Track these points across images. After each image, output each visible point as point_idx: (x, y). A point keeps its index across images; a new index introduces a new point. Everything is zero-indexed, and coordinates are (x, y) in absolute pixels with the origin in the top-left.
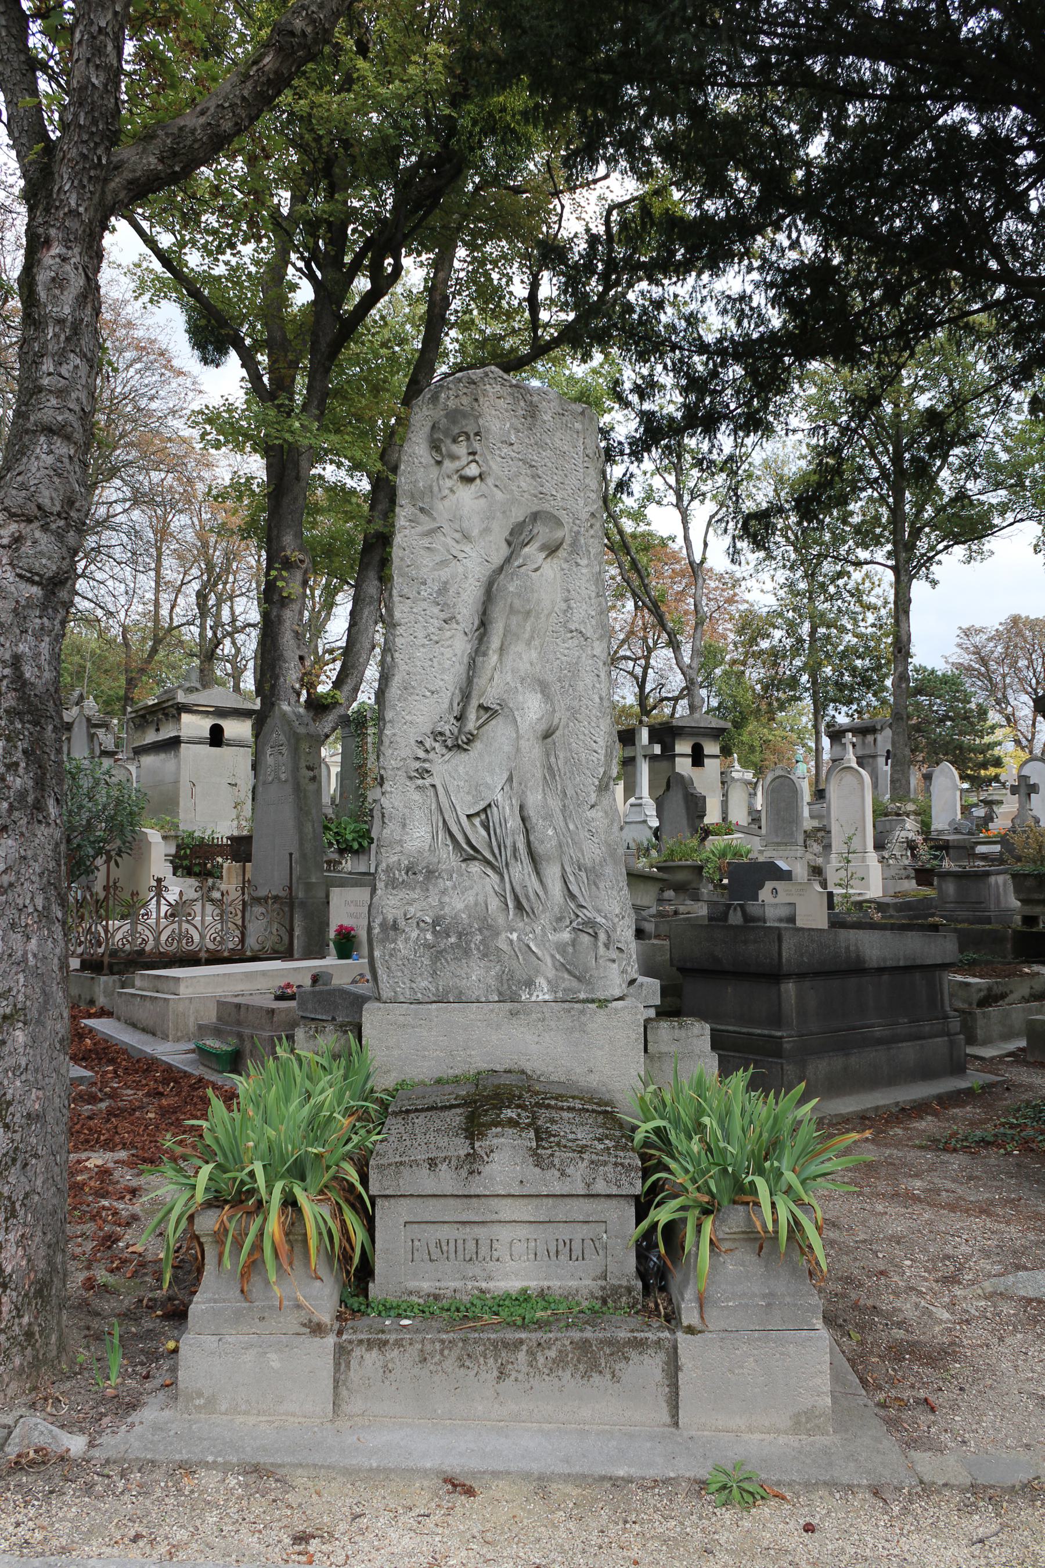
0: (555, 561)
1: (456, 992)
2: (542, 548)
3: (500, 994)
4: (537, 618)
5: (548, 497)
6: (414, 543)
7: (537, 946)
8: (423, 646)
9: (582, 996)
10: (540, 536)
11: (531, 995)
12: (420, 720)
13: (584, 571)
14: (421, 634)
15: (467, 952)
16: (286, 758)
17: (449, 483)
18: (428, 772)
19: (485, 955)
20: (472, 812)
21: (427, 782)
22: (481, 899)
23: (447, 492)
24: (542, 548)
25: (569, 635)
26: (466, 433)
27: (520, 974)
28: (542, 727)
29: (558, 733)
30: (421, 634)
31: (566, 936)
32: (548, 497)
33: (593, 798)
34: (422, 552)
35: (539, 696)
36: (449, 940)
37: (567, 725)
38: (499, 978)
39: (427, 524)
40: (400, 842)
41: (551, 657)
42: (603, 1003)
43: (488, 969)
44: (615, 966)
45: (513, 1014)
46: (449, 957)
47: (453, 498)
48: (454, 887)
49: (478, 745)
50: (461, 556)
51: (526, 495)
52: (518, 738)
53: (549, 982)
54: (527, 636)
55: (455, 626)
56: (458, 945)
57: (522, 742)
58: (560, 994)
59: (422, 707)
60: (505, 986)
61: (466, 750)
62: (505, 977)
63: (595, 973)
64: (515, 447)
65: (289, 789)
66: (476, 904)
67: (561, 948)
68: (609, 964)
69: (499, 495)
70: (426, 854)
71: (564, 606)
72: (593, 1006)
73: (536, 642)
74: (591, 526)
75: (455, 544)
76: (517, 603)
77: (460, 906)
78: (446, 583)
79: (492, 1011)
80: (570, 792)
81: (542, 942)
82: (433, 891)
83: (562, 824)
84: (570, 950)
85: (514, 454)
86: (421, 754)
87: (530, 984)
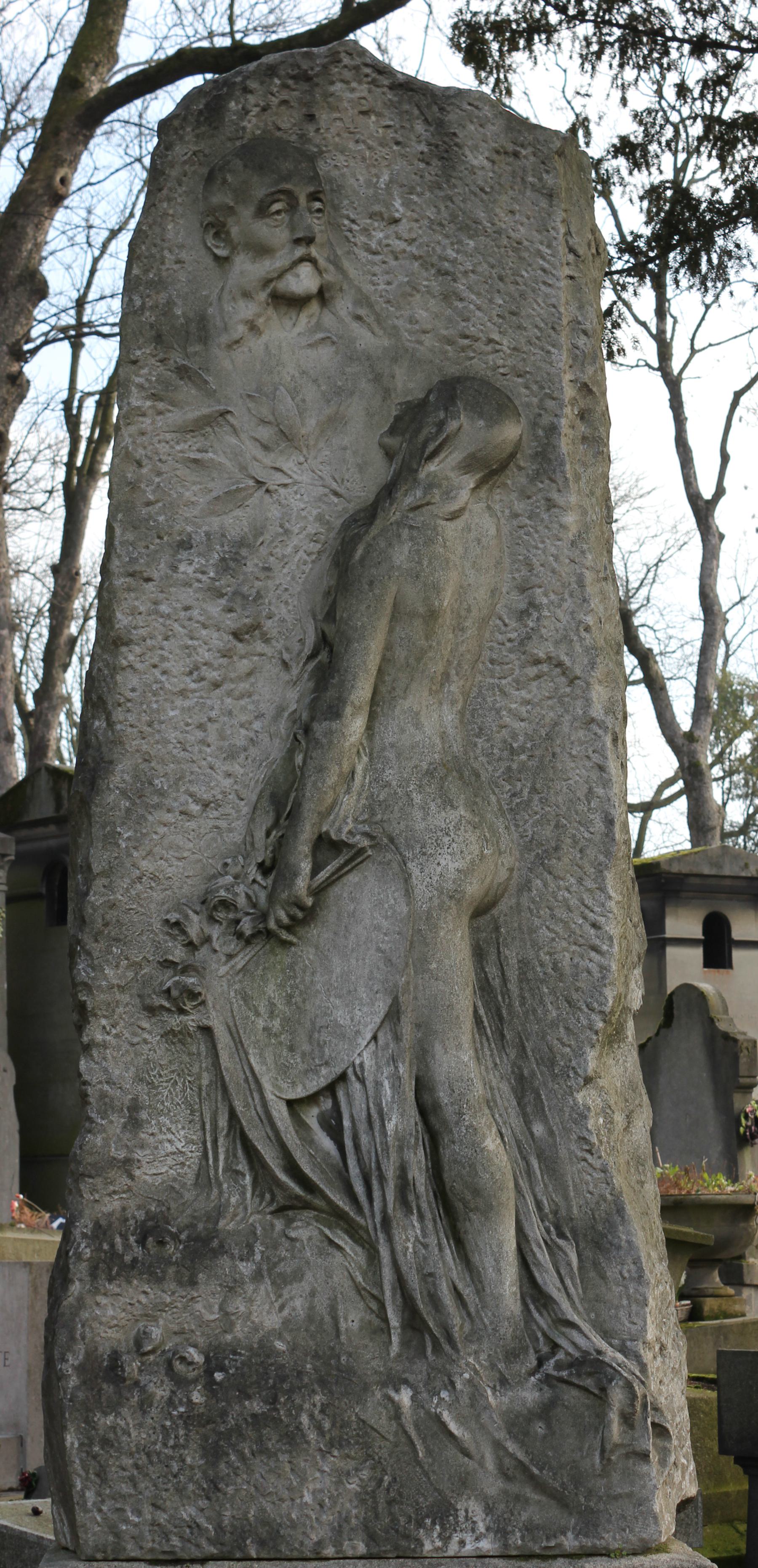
3: (371, 1538)
6: (163, 448)
7: (461, 1420)
8: (183, 693)
11: (446, 1540)
14: (176, 666)
17: (247, 310)
21: (191, 1021)
23: (241, 329)
25: (532, 671)
26: (289, 193)
30: (176, 666)
31: (530, 1395)
32: (480, 346)
34: (183, 472)
43: (341, 1476)
49: (313, 932)
53: (489, 1510)
55: (260, 647)
58: (516, 1539)
59: (179, 840)
66: (310, 1318)
75: (259, 453)
78: (242, 543)
87: (443, 1514)
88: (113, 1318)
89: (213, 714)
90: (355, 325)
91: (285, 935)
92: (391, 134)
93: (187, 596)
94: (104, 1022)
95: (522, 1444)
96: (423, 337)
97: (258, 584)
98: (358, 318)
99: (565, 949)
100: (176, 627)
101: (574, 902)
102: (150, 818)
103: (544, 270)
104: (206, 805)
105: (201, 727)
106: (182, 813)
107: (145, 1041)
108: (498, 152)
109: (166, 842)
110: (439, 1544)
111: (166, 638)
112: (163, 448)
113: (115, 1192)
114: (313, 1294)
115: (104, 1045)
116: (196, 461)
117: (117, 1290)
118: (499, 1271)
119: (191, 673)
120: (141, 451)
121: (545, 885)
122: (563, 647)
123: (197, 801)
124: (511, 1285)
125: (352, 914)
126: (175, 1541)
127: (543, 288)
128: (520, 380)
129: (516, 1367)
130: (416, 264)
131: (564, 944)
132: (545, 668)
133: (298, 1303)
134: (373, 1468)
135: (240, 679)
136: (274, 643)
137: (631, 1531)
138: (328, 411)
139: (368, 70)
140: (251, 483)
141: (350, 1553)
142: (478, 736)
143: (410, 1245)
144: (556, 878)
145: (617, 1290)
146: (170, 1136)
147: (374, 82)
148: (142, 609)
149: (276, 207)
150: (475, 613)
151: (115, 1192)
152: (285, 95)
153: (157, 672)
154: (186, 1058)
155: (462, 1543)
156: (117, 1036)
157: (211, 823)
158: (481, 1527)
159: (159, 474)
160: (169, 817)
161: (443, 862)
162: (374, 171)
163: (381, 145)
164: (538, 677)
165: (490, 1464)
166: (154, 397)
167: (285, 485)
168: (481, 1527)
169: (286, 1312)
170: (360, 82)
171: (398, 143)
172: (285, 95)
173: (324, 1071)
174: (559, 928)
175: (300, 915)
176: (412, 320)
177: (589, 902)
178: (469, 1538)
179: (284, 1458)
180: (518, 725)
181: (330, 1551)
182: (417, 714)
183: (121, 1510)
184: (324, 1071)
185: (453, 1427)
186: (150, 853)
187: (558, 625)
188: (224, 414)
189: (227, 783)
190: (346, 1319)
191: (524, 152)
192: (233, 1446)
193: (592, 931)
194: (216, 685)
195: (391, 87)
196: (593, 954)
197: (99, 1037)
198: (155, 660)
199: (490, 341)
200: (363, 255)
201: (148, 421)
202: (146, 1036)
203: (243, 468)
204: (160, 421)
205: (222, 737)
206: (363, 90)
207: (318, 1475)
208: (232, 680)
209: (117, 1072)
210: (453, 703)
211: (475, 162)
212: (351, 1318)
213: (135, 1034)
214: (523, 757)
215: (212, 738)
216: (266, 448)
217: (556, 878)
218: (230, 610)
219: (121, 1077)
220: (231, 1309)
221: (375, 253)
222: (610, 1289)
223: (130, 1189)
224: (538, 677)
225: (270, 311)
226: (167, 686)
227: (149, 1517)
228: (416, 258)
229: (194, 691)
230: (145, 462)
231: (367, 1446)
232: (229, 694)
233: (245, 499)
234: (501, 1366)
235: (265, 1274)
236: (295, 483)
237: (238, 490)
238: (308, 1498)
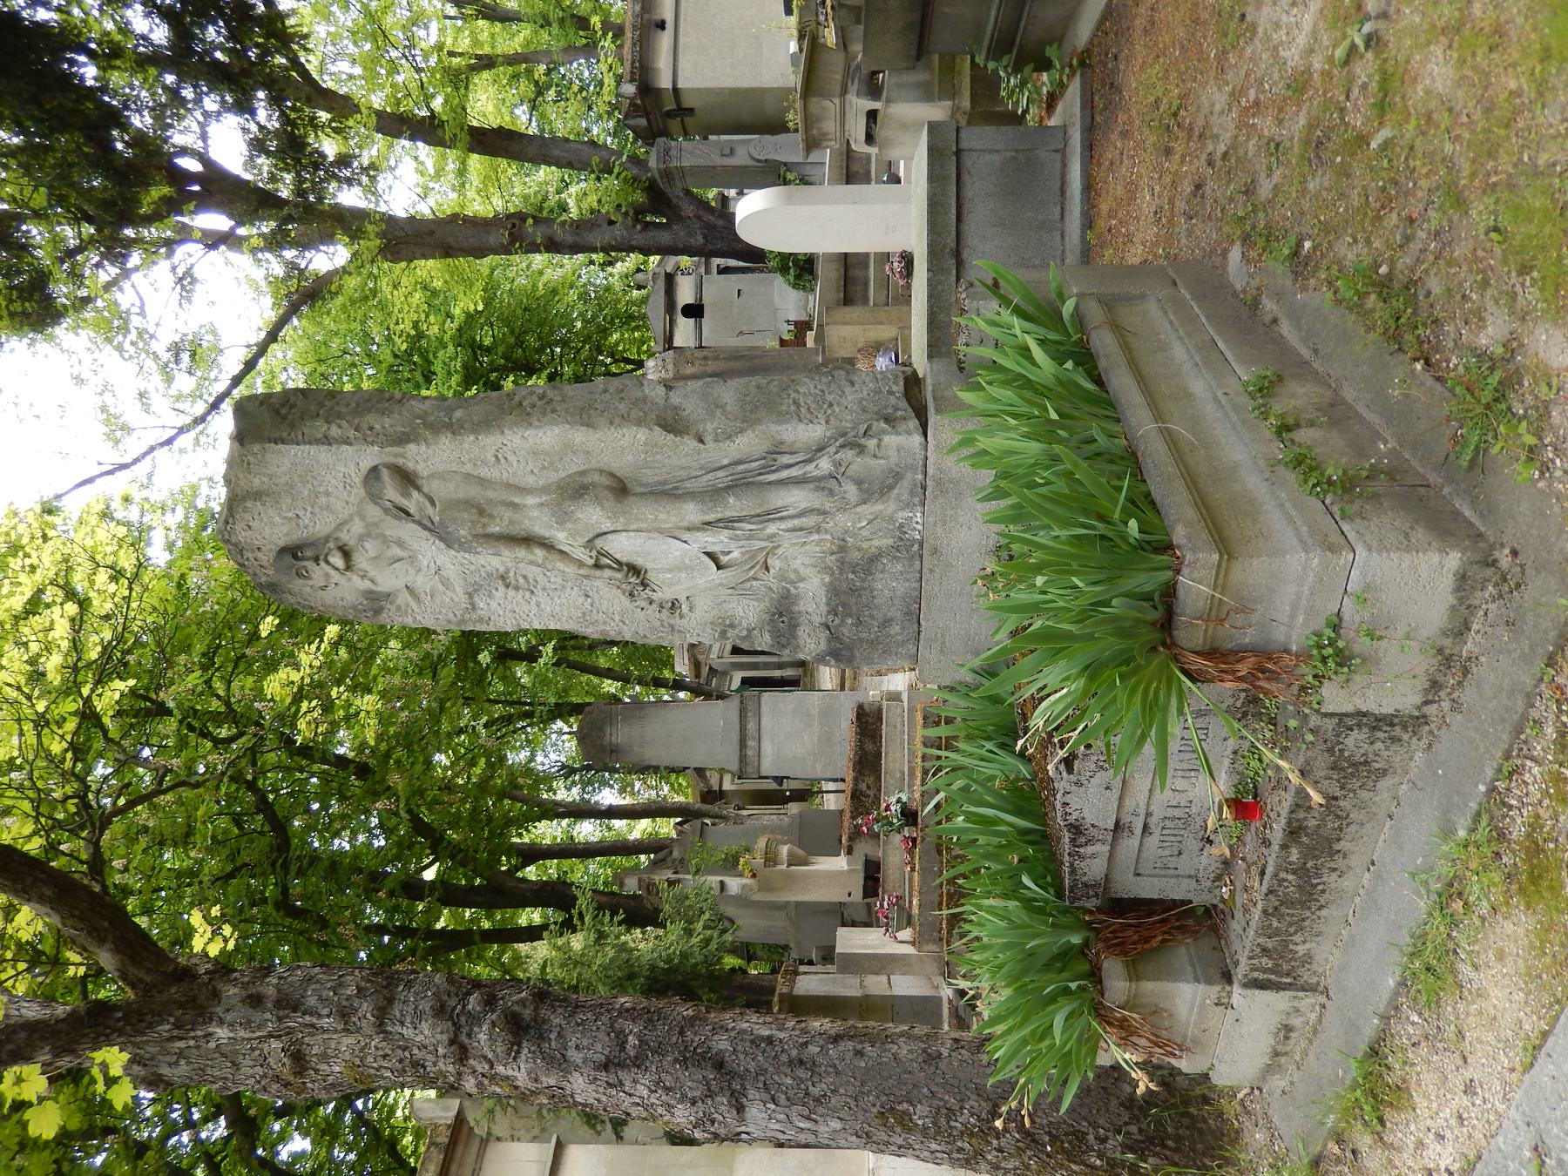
2: (407, 495)
28: (610, 502)
34: (438, 601)
79: (931, 571)
83: (720, 474)
93: (494, 605)
206: (238, 527)
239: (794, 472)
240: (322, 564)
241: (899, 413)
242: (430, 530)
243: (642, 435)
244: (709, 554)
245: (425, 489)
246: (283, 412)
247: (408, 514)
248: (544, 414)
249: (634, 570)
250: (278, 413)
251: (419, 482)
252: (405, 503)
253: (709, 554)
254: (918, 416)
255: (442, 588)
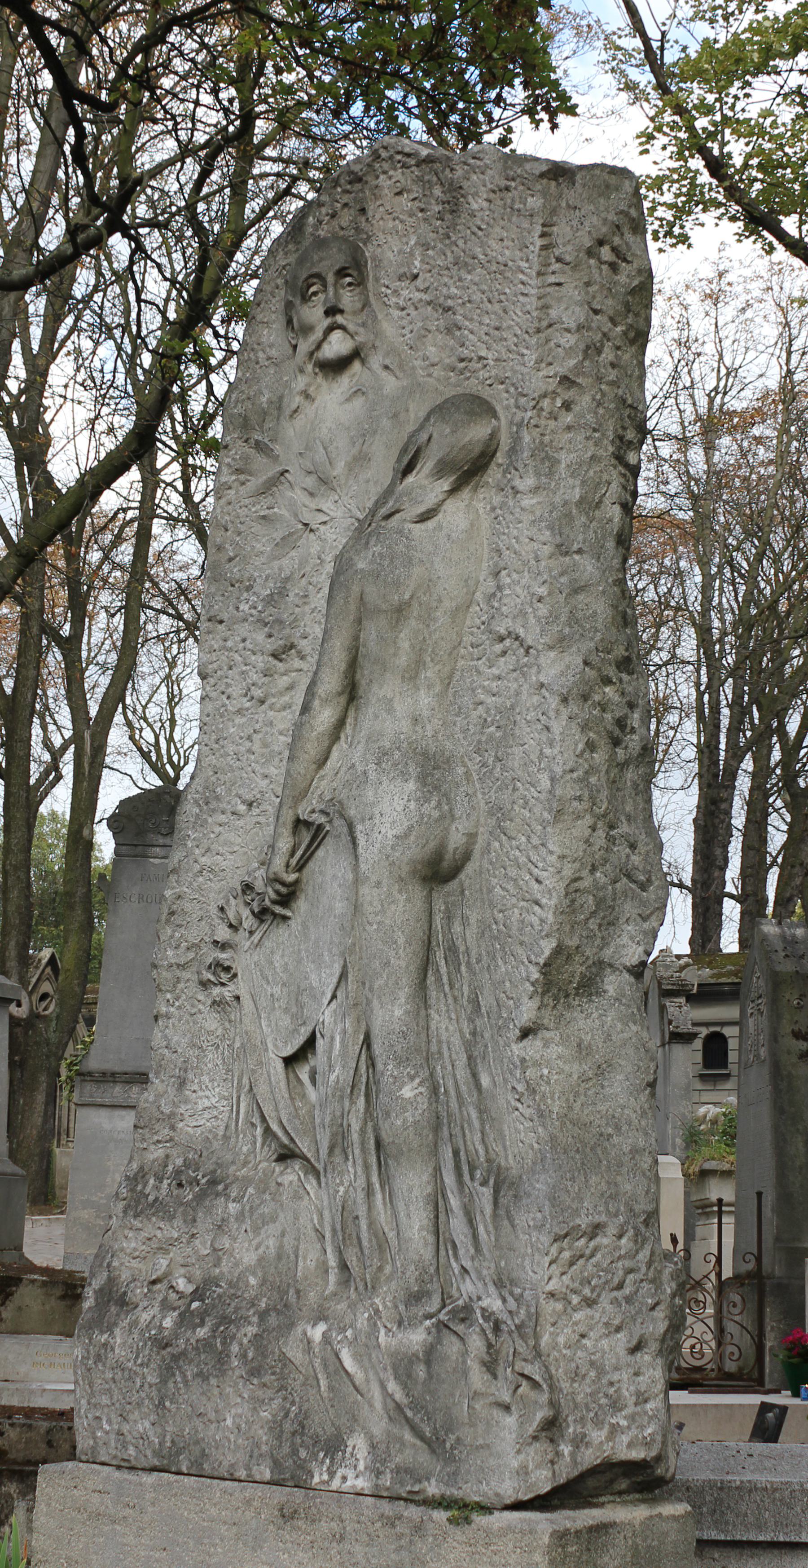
0: (482, 493)
1: (196, 1450)
2: (440, 471)
3: (276, 1465)
4: (427, 618)
5: (475, 365)
6: (242, 512)
7: (357, 1357)
8: (240, 712)
9: (433, 1489)
10: (433, 445)
11: (332, 1474)
12: (227, 862)
13: (527, 502)
14: (236, 691)
15: (222, 1359)
16: (764, 1021)
17: (301, 382)
18: (227, 969)
19: (255, 1372)
20: (289, 1051)
21: (227, 993)
22: (289, 1242)
23: (298, 399)
24: (440, 471)
25: (498, 648)
26: (318, 276)
27: (321, 1423)
28: (414, 851)
29: (470, 868)
30: (236, 691)
31: (417, 1338)
32: (475, 365)
33: (527, 1011)
34: (257, 528)
35: (411, 785)
36: (218, 1328)
37: (487, 850)
38: (276, 1428)
39: (265, 470)
40: (171, 1121)
41: (467, 700)
42: (463, 1510)
43: (257, 1403)
44: (510, 1420)
45: (287, 1515)
46: (190, 1371)
47: (309, 410)
48: (240, 1217)
49: (301, 905)
50: (315, 520)
51: (437, 372)
52: (357, 881)
53: (373, 1446)
54: (402, 660)
55: (297, 663)
56: (206, 1345)
57: (365, 890)
58: (387, 1480)
59: (232, 837)
60: (286, 1449)
61: (285, 918)
62: (288, 1427)
63: (466, 1434)
64: (419, 282)
65: (766, 1071)
66: (279, 1257)
67: (402, 1366)
68: (497, 1413)
69: (391, 384)
70: (216, 1145)
71: (490, 585)
72: (440, 1516)
73: (430, 673)
74: (567, 406)
75: (307, 500)
76: (373, 593)
77: (249, 1258)
78: (287, 579)
79: (248, 1502)
80: (486, 1001)
81: (365, 1349)
82: (204, 1224)
83: (462, 1073)
84: (421, 1372)
85: (418, 295)
86: (223, 933)
87: (334, 1447)
88: (135, 1249)
89: (257, 727)
90: (384, 374)
91: (278, 909)
92: (417, 204)
93: (243, 630)
94: (169, 996)
95: (404, 1386)
96: (432, 370)
97: (297, 610)
98: (386, 367)
99: (514, 906)
100: (237, 657)
101: (523, 860)
102: (210, 820)
103: (523, 283)
104: (250, 805)
105: (249, 738)
106: (233, 813)
107: (200, 1012)
108: (494, 192)
109: (221, 838)
110: (325, 1477)
111: (230, 668)
112: (242, 512)
113: (158, 1142)
114: (283, 1235)
115: (168, 1016)
116: (264, 517)
117: (140, 1225)
118: (408, 1216)
119: (246, 695)
120: (227, 518)
121: (501, 845)
122: (520, 621)
123: (243, 802)
124: (421, 1229)
125: (321, 887)
126: (132, 1451)
127: (521, 298)
128: (501, 387)
129: (414, 1310)
130: (429, 308)
131: (514, 900)
132: (507, 642)
133: (271, 1242)
134: (285, 1399)
135: (281, 694)
136: (309, 658)
137: (488, 1484)
138: (355, 451)
139: (399, 157)
140: (300, 526)
141: (258, 1478)
142: (458, 715)
143: (342, 1189)
144: (510, 838)
145: (524, 1238)
146: (207, 1093)
147: (405, 166)
148: (216, 647)
149: (313, 289)
150: (447, 604)
151: (158, 1142)
152: (346, 199)
153: (224, 697)
154: (227, 1025)
155: (344, 1479)
156: (179, 1008)
157: (254, 820)
158: (361, 1466)
159: (239, 534)
160: (222, 818)
161: (383, 831)
162: (404, 240)
163: (411, 216)
164: (504, 653)
165: (378, 1405)
166: (239, 471)
167: (325, 523)
168: (361, 1466)
169: (261, 1251)
170: (395, 169)
171: (422, 210)
172: (346, 199)
173: (303, 1030)
174: (510, 886)
175: (284, 890)
176: (425, 358)
177: (534, 858)
178: (351, 1474)
179: (213, 1381)
180: (490, 700)
181: (242, 1474)
182: (391, 700)
183: (98, 1418)
184: (303, 1030)
185: (349, 1363)
186: (208, 850)
187: (518, 601)
188: (283, 473)
189: (264, 783)
190: (305, 1258)
191: (513, 184)
192: (179, 1368)
193: (536, 886)
194: (262, 702)
195: (417, 165)
196: (536, 908)
197: (164, 1009)
198: (223, 688)
199: (481, 358)
200: (396, 313)
201: (232, 492)
202: (201, 1007)
203: (296, 515)
204: (243, 490)
205: (265, 745)
206: (397, 174)
207: (239, 1400)
208: (273, 696)
209: (175, 1038)
210: (430, 687)
211: (475, 206)
212: (310, 1257)
213: (193, 1006)
214: (492, 729)
215: (256, 747)
216: (312, 494)
217: (510, 838)
218: (270, 636)
219: (178, 1043)
220: (217, 1246)
221: (403, 309)
222: (517, 1237)
223: (171, 1140)
224: (504, 653)
225: (320, 379)
226: (230, 708)
227: (116, 1427)
228: (429, 303)
229: (247, 709)
230: (230, 526)
231: (282, 1377)
232: (271, 708)
233: (296, 541)
234: (402, 1307)
235: (247, 1214)
236: (332, 519)
237: (291, 534)
238: (229, 1422)
239: (457, 1226)
240: (327, 322)
241: (566, 1449)
242: (373, 512)
243: (546, 914)
244: (310, 1044)
245: (450, 505)
246: (606, 253)
247: (408, 470)
248: (585, 727)
249: (288, 897)
250: (601, 243)
251: (466, 493)
252: (426, 466)
253: (310, 1044)
254: (556, 1492)
255: (278, 535)
